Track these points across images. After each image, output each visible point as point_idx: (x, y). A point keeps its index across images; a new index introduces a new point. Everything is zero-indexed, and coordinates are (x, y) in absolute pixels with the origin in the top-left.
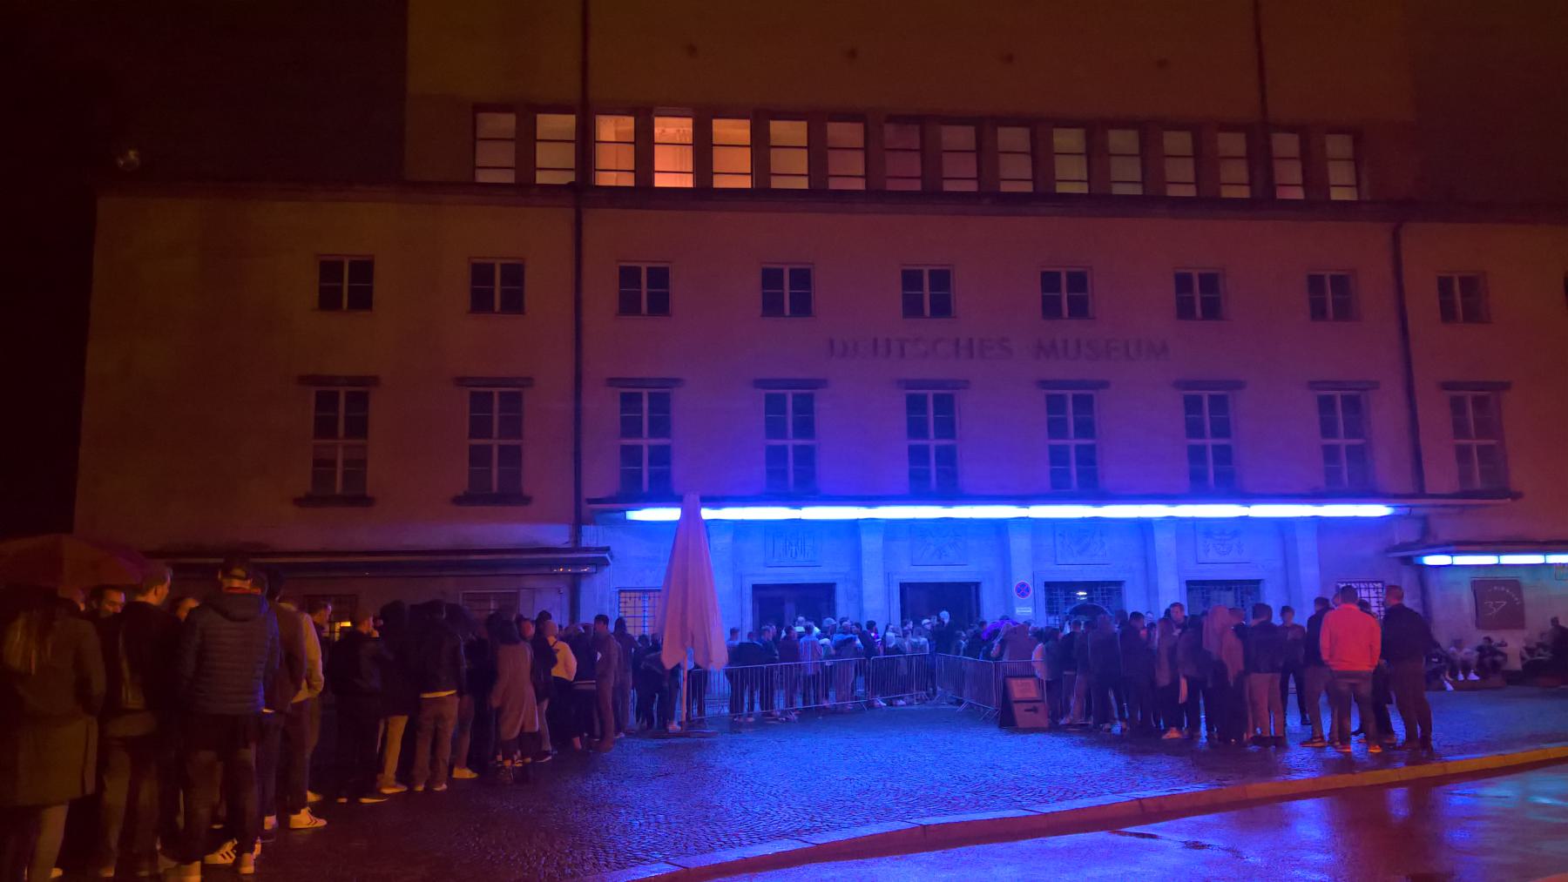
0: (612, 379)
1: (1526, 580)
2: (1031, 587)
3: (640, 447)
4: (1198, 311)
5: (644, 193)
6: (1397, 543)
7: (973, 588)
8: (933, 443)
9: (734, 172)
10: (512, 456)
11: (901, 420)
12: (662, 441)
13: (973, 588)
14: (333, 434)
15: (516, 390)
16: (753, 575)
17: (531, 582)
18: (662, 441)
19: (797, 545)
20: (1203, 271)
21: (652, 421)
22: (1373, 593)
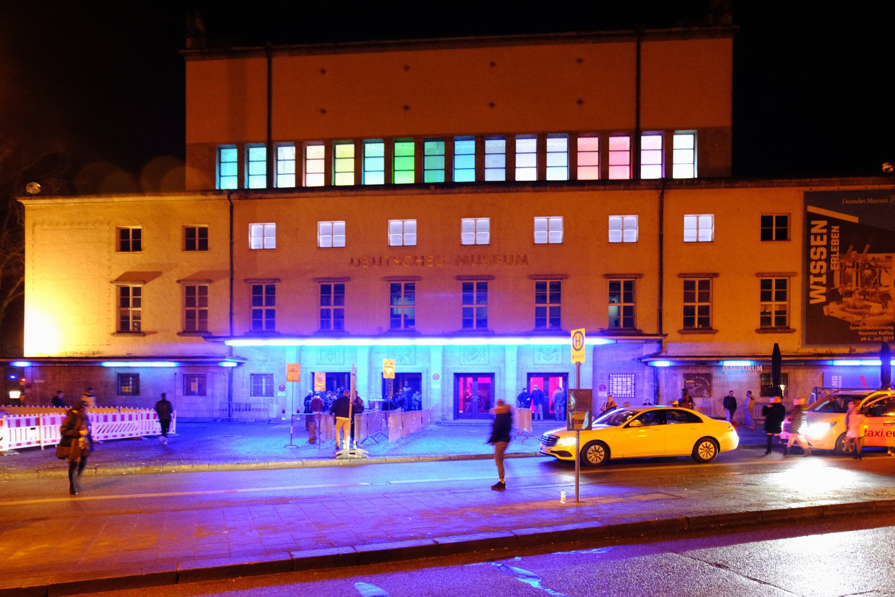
0: (607, 275)
1: (142, 374)
2: (441, 376)
3: (472, 309)
4: (197, 246)
5: (510, 183)
6: (644, 354)
7: (346, 375)
8: (475, 306)
9: (557, 172)
10: (204, 314)
11: (533, 292)
12: (324, 307)
13: (346, 376)
14: (770, 299)
15: (559, 280)
16: (311, 368)
17: (212, 370)
18: (324, 307)
19: (332, 354)
20: (778, 215)
21: (267, 298)
22: (629, 379)
